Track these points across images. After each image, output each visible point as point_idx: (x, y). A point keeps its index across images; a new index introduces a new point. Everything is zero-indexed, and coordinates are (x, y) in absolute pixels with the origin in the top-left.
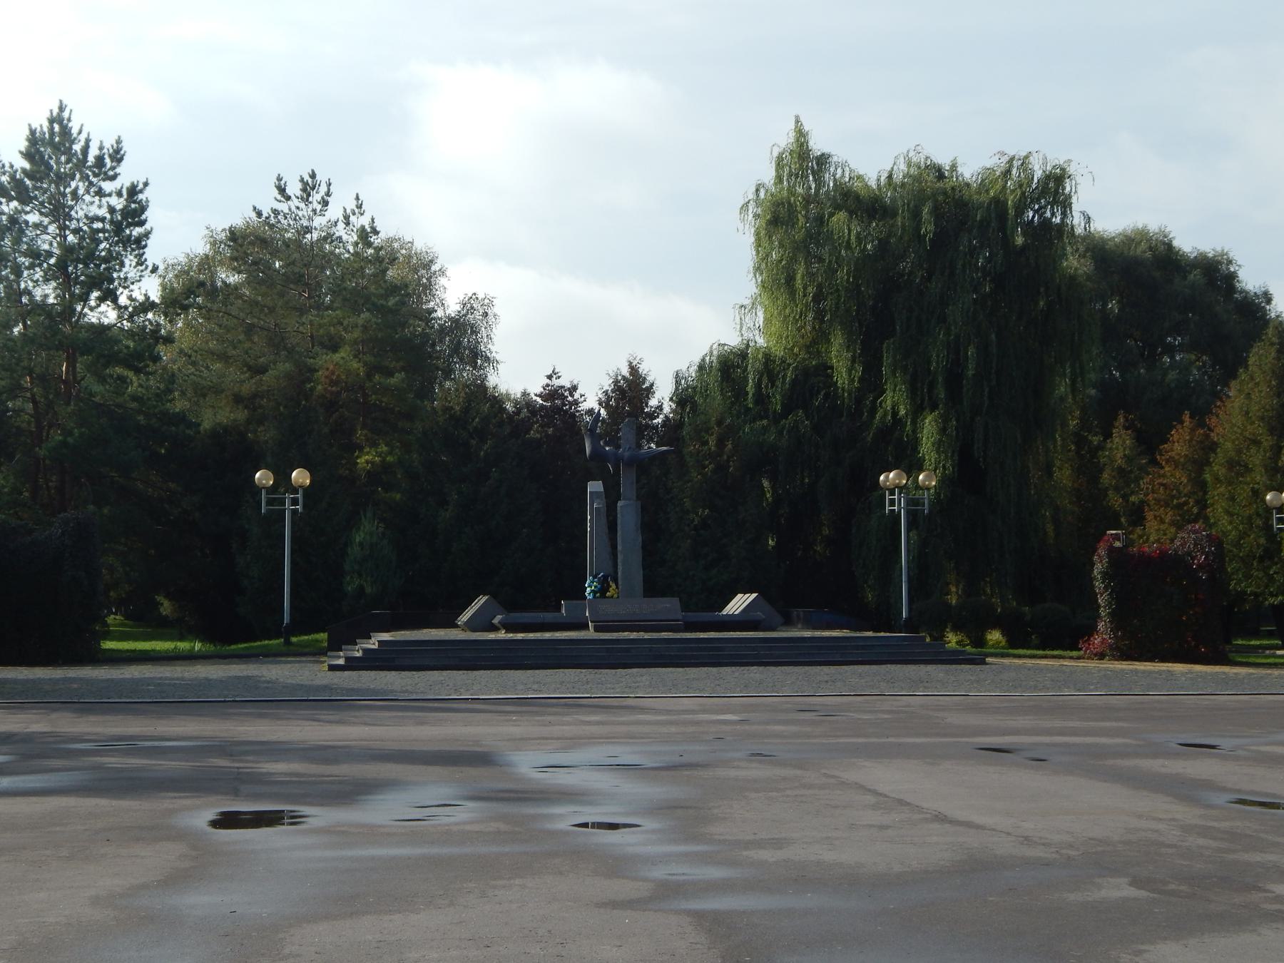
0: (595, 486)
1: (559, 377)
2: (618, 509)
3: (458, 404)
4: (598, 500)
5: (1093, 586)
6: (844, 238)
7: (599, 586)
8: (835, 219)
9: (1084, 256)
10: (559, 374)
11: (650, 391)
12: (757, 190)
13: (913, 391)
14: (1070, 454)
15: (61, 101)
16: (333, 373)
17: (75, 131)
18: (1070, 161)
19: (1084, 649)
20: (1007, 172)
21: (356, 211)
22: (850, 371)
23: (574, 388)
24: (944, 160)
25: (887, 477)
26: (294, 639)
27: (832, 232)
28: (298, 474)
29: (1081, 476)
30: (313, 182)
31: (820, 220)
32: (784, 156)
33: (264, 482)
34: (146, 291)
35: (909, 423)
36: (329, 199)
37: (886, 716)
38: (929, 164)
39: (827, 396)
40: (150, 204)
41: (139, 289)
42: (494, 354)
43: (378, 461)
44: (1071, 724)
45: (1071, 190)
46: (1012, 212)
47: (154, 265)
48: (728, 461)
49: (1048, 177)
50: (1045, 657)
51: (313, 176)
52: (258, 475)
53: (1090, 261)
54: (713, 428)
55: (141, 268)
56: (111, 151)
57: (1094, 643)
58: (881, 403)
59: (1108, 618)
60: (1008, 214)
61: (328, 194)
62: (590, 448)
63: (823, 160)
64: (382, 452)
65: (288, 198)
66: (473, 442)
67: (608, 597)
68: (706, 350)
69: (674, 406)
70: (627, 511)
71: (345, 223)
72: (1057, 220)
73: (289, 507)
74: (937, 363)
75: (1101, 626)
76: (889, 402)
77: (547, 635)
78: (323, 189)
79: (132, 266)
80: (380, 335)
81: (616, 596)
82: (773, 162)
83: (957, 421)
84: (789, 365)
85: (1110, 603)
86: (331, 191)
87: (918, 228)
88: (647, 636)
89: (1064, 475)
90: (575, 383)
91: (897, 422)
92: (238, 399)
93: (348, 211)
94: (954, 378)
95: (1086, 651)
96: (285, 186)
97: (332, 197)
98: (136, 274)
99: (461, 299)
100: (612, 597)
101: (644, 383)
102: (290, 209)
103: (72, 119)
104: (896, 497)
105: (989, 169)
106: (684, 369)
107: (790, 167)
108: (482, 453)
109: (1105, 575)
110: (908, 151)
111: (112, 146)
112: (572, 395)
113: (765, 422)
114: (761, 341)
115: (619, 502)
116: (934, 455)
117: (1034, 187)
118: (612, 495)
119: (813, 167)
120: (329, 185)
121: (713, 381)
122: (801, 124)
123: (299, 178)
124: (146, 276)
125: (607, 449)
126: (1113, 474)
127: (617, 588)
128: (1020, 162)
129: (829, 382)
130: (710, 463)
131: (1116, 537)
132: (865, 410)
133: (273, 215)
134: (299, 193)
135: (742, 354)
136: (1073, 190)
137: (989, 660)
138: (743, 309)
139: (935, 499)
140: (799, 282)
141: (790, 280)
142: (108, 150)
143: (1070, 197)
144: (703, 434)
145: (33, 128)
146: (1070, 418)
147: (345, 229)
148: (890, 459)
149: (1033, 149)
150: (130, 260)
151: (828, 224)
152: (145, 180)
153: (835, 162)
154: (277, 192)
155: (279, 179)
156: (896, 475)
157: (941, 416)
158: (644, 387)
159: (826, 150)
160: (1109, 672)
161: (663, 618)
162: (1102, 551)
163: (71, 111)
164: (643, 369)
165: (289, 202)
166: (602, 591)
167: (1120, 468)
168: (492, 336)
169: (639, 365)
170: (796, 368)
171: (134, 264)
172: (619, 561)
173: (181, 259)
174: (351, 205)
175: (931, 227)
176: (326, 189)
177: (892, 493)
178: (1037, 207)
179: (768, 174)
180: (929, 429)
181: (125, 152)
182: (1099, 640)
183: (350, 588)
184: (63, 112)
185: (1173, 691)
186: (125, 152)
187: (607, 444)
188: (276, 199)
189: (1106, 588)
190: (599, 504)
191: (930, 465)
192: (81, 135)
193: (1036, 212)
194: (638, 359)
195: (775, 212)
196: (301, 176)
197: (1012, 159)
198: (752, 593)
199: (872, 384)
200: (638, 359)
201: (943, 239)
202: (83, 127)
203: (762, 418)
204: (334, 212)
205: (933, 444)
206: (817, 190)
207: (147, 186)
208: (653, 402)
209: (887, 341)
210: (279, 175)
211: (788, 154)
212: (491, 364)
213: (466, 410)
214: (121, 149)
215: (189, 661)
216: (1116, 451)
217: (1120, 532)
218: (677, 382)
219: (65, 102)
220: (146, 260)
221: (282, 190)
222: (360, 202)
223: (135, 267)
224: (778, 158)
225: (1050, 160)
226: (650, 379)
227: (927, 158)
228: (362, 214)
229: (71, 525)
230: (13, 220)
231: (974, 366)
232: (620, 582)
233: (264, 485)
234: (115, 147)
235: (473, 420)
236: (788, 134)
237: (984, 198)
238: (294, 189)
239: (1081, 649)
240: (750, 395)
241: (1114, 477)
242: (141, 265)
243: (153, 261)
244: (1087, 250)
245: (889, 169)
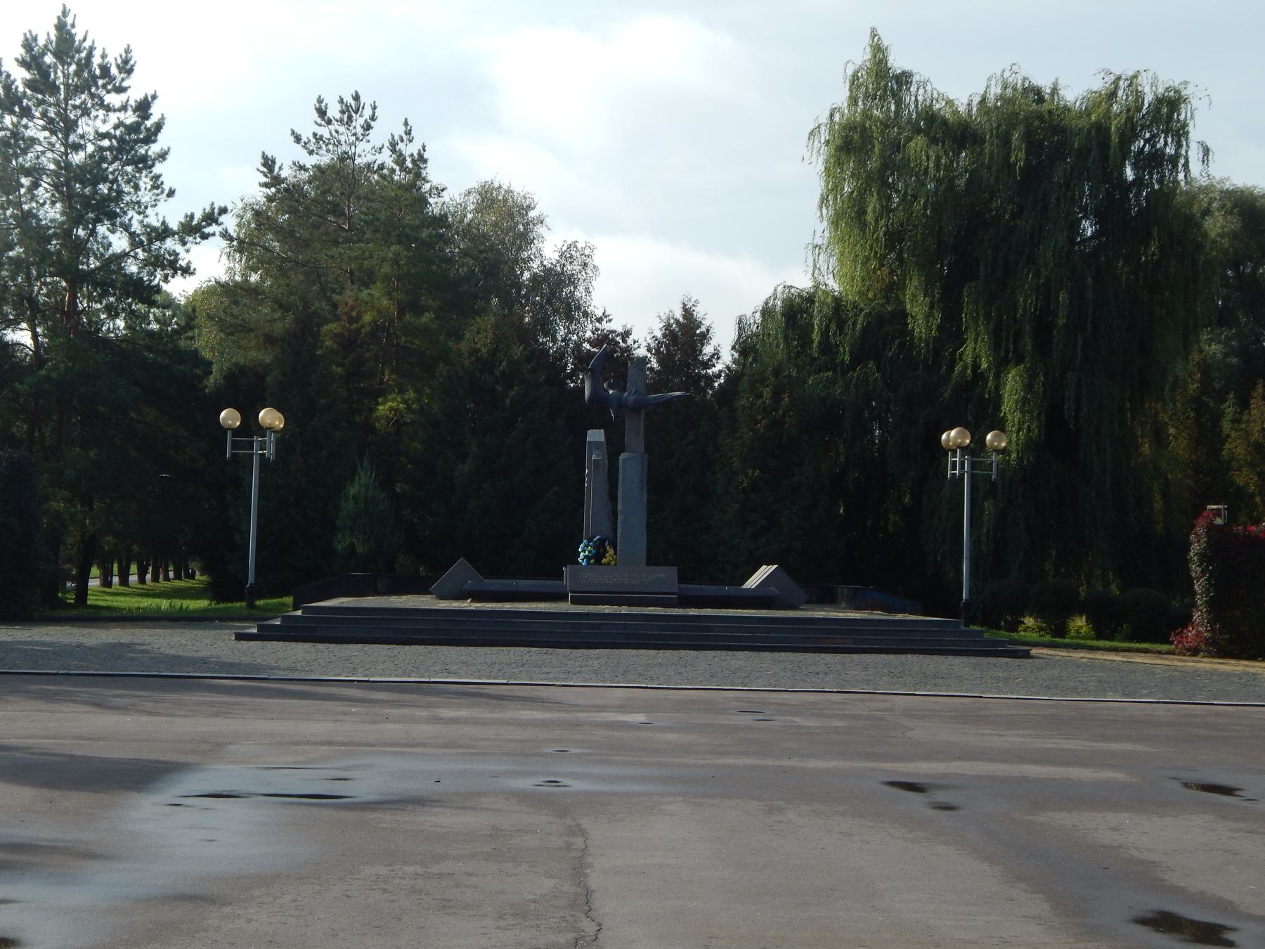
0: (596, 435)
1: (610, 321)
2: (620, 462)
3: (485, 345)
4: (598, 452)
5: (1189, 570)
6: (921, 166)
7: (594, 551)
8: (912, 144)
9: (1231, 213)
10: (610, 317)
11: (705, 337)
12: (832, 115)
14: (1189, 422)
15: (64, 5)
16: (352, 309)
17: (78, 38)
18: (1186, 82)
19: (1175, 642)
20: (1112, 95)
21: (405, 137)
22: (927, 317)
23: (626, 334)
24: (1043, 82)
25: (949, 436)
26: (260, 603)
27: (909, 159)
28: (265, 413)
29: (1200, 447)
30: (356, 104)
31: (897, 146)
32: (860, 74)
33: (230, 422)
34: (164, 217)
35: (991, 378)
36: (372, 123)
37: (839, 723)
38: (1027, 86)
39: (902, 345)
40: (166, 121)
41: (157, 215)
42: (592, 308)
43: (402, 409)
44: (1070, 745)
45: (1186, 116)
46: (1115, 138)
47: (170, 189)
48: (784, 416)
49: (1159, 101)
50: (1146, 651)
51: (357, 98)
52: (223, 414)
53: (1238, 218)
54: (769, 379)
55: (156, 191)
56: (119, 61)
57: (1187, 636)
58: (961, 355)
59: (1205, 607)
60: (1111, 141)
61: (373, 118)
62: (589, 390)
63: (904, 79)
64: (409, 399)
65: (329, 122)
66: (499, 388)
67: (604, 564)
68: (769, 293)
69: (736, 355)
70: (631, 465)
71: (391, 151)
72: (1170, 150)
73: (257, 451)
74: (1025, 310)
75: (1197, 616)
76: (969, 352)
77: (507, 606)
78: (367, 112)
79: (147, 189)
80: (413, 271)
81: (613, 563)
82: (848, 81)
83: (1046, 375)
84: (861, 310)
85: (1207, 589)
86: (376, 115)
87: (1008, 156)
88: (624, 610)
89: (1180, 443)
90: (629, 327)
91: (978, 376)
92: (270, 340)
93: (397, 138)
94: (1043, 327)
95: (1177, 646)
96: (326, 108)
97: (376, 121)
98: (151, 198)
99: (560, 246)
100: (609, 564)
101: (699, 327)
102: (331, 134)
103: (76, 25)
104: (957, 459)
105: (1095, 92)
106: (749, 314)
107: (867, 87)
108: (508, 401)
109: (1203, 557)
110: (1004, 71)
111: (121, 56)
112: (624, 341)
113: (829, 374)
114: (834, 285)
115: (622, 454)
116: (1018, 415)
117: (1144, 113)
118: (615, 446)
119: (892, 88)
120: (374, 108)
121: (776, 327)
122: (879, 38)
123: (338, 99)
124: (162, 201)
125: (611, 392)
126: (1249, 449)
127: (615, 554)
128: (1127, 83)
129: (905, 332)
130: (763, 418)
131: (1217, 513)
132: (944, 363)
133: (313, 140)
134: (338, 116)
135: (810, 299)
136: (1189, 116)
137: (1034, 651)
138: (817, 249)
139: (1017, 465)
140: (870, 217)
141: (862, 212)
142: (116, 59)
143: (1185, 125)
144: (758, 385)
145: (34, 35)
146: (1190, 381)
147: (391, 156)
148: (970, 418)
149: (1141, 68)
150: (145, 181)
151: (904, 150)
152: (153, 93)
153: (917, 82)
154: (317, 115)
155: (320, 101)
156: (958, 433)
157: (1027, 370)
158: (698, 332)
159: (907, 68)
160: (1177, 673)
161: (666, 591)
162: (1200, 530)
163: (75, 16)
164: (699, 312)
165: (330, 126)
166: (597, 557)
167: (1257, 442)
168: (591, 289)
169: (694, 308)
170: (869, 314)
171: (149, 187)
172: (619, 521)
173: (259, 199)
174: (399, 131)
175: (1022, 155)
176: (371, 113)
177: (954, 455)
178: (1148, 135)
179: (840, 96)
180: (1012, 385)
181: (135, 62)
182: (1194, 632)
183: (339, 547)
184: (67, 17)
185: (1246, 700)
186: (135, 62)
187: (610, 386)
188: (316, 123)
189: (1203, 572)
190: (598, 456)
191: (1013, 426)
192: (86, 42)
193: (1147, 141)
194: (693, 300)
195: (847, 137)
196: (340, 97)
197: (1119, 78)
199: (951, 334)
200: (693, 300)
201: (1033, 173)
202: (88, 34)
203: (828, 369)
204: (380, 135)
205: (1017, 402)
206: (897, 112)
207: (155, 99)
208: (708, 350)
209: (968, 284)
210: (320, 96)
211: (864, 73)
212: (589, 319)
213: (493, 353)
214: (130, 59)
215: (123, 623)
216: (1252, 425)
217: (1220, 507)
218: (740, 328)
219: (68, 7)
220: (162, 183)
221: (322, 113)
222: (409, 128)
223: (150, 191)
224: (853, 76)
225: (1163, 82)
226: (706, 323)
227: (1025, 79)
228: (411, 141)
229: (4, 465)
230: (15, 135)
231: (1066, 313)
232: (618, 548)
233: (230, 425)
234: (123, 57)
235: (500, 364)
236: (865, 49)
237: (1083, 123)
238: (334, 111)
239: (1171, 643)
240: (815, 345)
241: (1249, 452)
242: (157, 188)
243: (172, 185)
244: (1235, 205)
245: (982, 93)
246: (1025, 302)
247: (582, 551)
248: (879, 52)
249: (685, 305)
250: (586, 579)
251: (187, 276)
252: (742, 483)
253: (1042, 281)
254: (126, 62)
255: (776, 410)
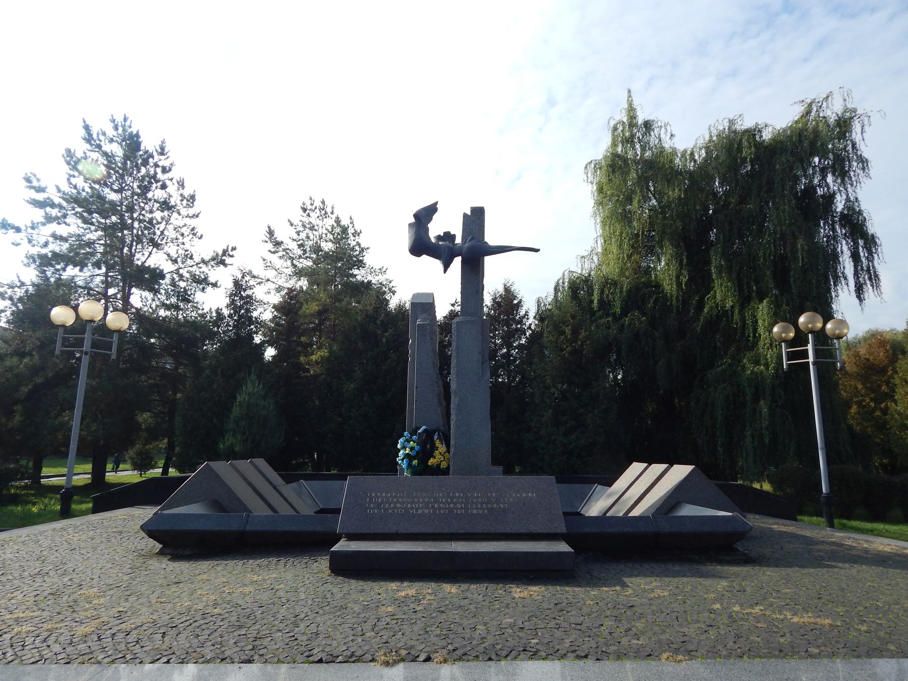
7: (417, 448)
11: (519, 304)
13: (739, 285)
39: (656, 300)
48: (582, 345)
68: (560, 275)
74: (765, 259)
106: (544, 297)
119: (639, 137)
120: (333, 208)
127: (448, 451)
172: (452, 406)
190: (424, 320)
197: (810, 105)
198: (671, 460)
218: (538, 305)
219: (127, 116)
226: (519, 297)
232: (452, 442)
246: (765, 253)
247: (402, 448)
248: (631, 111)
249: (505, 285)
250: (378, 506)
251: (215, 288)
252: (554, 394)
253: (778, 236)
254: (162, 148)
255: (576, 342)
